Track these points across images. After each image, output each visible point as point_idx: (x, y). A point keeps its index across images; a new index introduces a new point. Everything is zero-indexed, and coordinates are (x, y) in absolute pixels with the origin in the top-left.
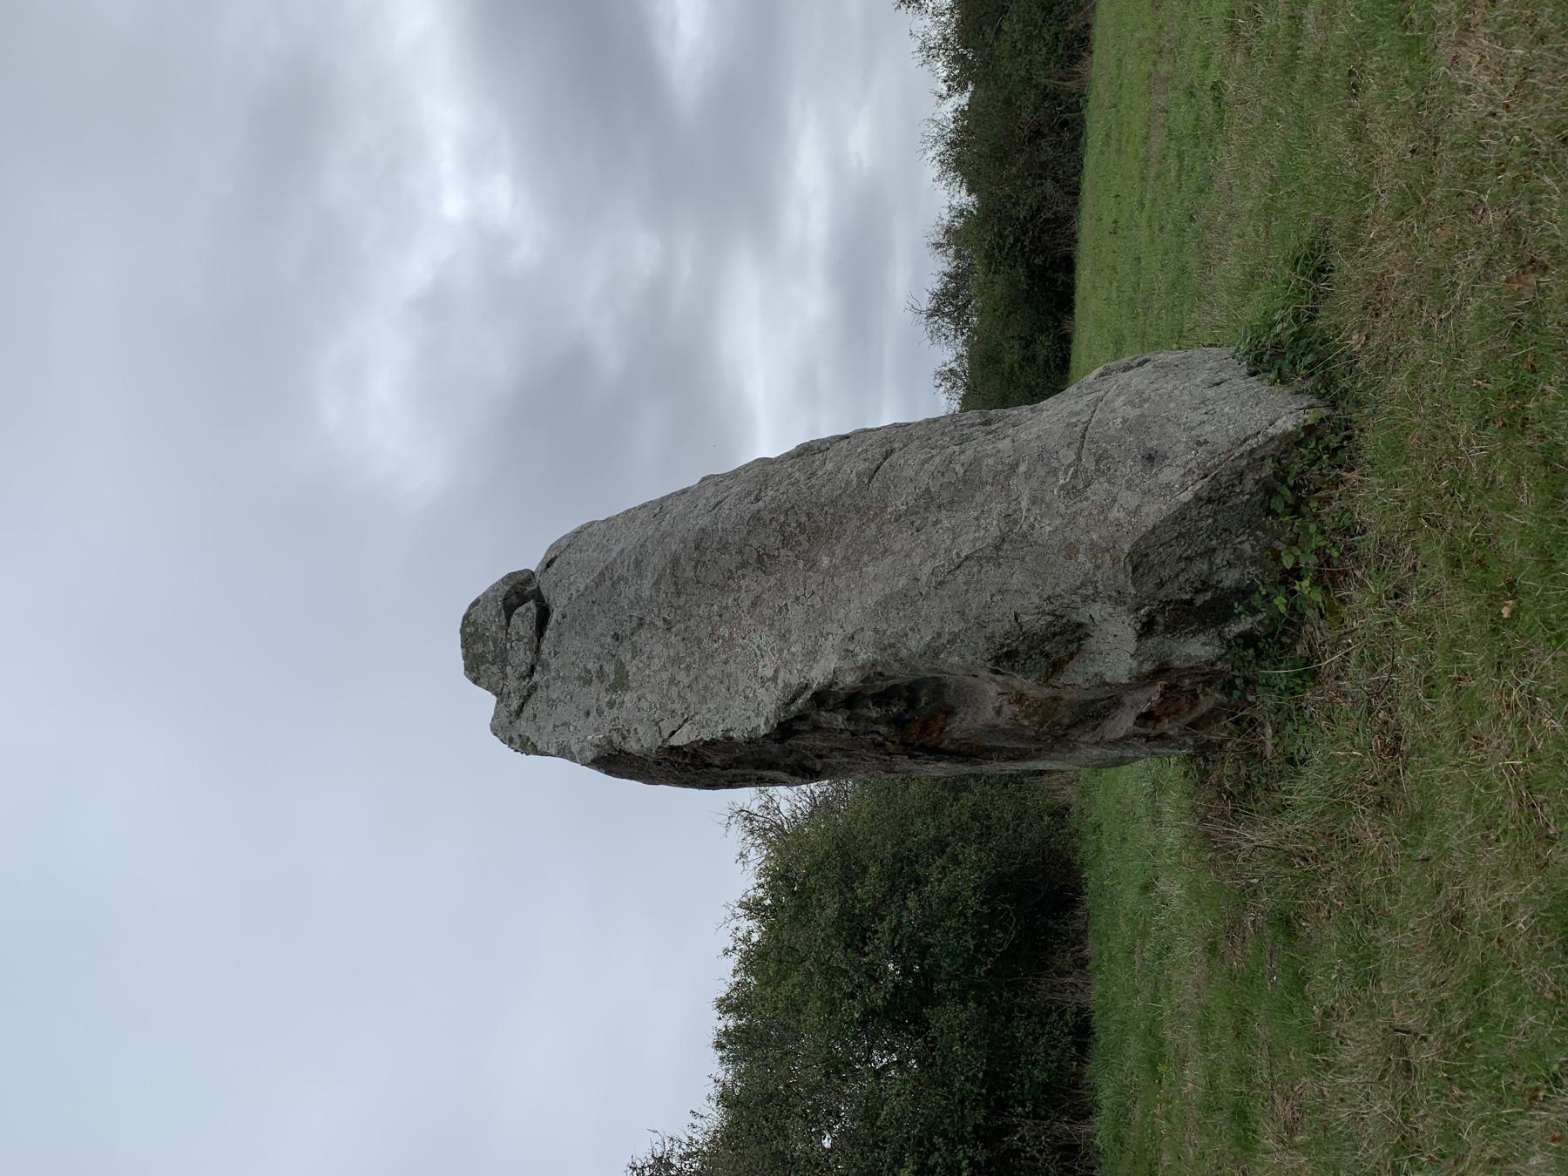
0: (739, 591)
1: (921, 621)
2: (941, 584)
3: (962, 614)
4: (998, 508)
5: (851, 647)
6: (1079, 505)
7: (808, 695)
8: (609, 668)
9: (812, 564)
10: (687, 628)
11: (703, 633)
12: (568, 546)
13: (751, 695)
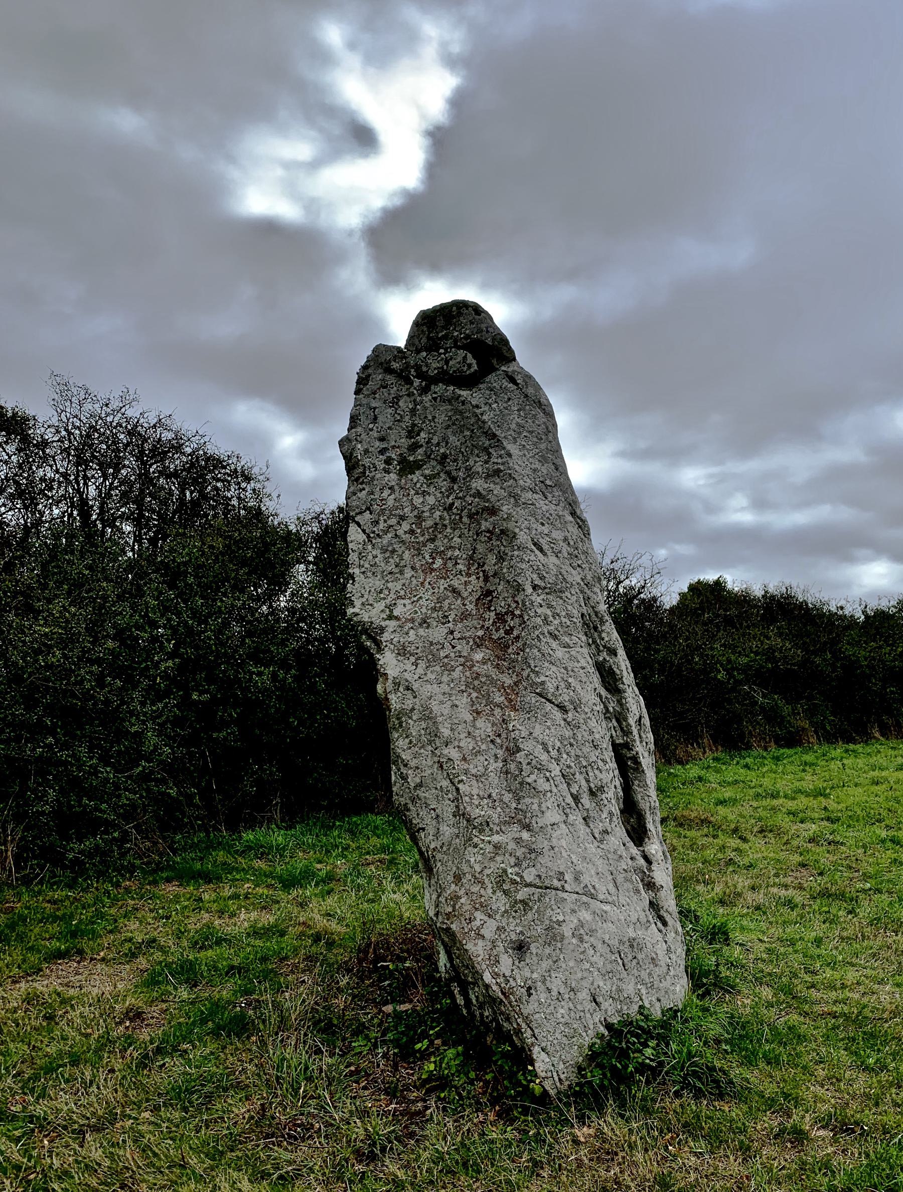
0: (467, 574)
1: (417, 749)
3: (420, 785)
4: (495, 816)
5: (401, 689)
6: (490, 886)
8: (420, 454)
9: (479, 644)
10: (446, 526)
11: (440, 544)
12: (526, 396)
13: (382, 596)
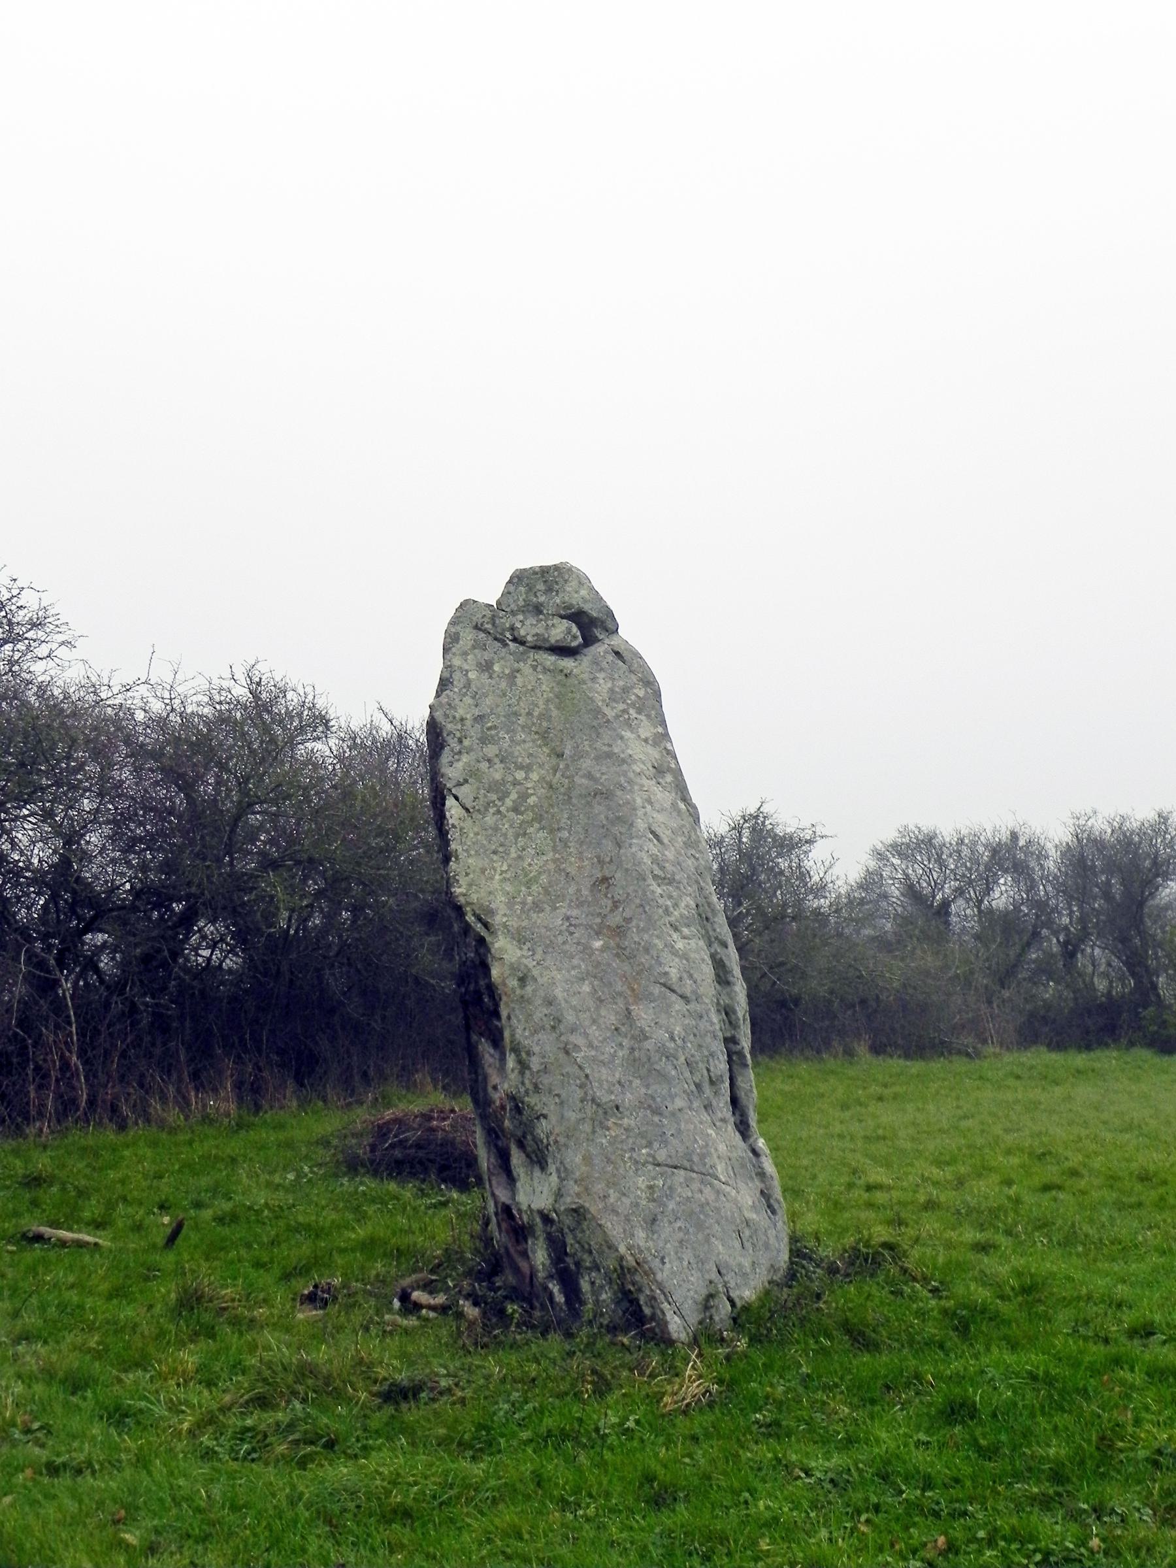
2: (567, 1053)
7: (484, 932)
